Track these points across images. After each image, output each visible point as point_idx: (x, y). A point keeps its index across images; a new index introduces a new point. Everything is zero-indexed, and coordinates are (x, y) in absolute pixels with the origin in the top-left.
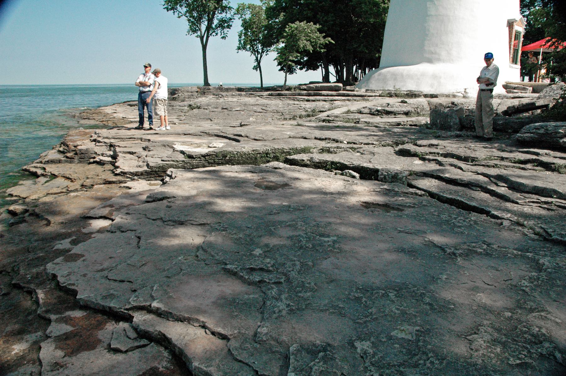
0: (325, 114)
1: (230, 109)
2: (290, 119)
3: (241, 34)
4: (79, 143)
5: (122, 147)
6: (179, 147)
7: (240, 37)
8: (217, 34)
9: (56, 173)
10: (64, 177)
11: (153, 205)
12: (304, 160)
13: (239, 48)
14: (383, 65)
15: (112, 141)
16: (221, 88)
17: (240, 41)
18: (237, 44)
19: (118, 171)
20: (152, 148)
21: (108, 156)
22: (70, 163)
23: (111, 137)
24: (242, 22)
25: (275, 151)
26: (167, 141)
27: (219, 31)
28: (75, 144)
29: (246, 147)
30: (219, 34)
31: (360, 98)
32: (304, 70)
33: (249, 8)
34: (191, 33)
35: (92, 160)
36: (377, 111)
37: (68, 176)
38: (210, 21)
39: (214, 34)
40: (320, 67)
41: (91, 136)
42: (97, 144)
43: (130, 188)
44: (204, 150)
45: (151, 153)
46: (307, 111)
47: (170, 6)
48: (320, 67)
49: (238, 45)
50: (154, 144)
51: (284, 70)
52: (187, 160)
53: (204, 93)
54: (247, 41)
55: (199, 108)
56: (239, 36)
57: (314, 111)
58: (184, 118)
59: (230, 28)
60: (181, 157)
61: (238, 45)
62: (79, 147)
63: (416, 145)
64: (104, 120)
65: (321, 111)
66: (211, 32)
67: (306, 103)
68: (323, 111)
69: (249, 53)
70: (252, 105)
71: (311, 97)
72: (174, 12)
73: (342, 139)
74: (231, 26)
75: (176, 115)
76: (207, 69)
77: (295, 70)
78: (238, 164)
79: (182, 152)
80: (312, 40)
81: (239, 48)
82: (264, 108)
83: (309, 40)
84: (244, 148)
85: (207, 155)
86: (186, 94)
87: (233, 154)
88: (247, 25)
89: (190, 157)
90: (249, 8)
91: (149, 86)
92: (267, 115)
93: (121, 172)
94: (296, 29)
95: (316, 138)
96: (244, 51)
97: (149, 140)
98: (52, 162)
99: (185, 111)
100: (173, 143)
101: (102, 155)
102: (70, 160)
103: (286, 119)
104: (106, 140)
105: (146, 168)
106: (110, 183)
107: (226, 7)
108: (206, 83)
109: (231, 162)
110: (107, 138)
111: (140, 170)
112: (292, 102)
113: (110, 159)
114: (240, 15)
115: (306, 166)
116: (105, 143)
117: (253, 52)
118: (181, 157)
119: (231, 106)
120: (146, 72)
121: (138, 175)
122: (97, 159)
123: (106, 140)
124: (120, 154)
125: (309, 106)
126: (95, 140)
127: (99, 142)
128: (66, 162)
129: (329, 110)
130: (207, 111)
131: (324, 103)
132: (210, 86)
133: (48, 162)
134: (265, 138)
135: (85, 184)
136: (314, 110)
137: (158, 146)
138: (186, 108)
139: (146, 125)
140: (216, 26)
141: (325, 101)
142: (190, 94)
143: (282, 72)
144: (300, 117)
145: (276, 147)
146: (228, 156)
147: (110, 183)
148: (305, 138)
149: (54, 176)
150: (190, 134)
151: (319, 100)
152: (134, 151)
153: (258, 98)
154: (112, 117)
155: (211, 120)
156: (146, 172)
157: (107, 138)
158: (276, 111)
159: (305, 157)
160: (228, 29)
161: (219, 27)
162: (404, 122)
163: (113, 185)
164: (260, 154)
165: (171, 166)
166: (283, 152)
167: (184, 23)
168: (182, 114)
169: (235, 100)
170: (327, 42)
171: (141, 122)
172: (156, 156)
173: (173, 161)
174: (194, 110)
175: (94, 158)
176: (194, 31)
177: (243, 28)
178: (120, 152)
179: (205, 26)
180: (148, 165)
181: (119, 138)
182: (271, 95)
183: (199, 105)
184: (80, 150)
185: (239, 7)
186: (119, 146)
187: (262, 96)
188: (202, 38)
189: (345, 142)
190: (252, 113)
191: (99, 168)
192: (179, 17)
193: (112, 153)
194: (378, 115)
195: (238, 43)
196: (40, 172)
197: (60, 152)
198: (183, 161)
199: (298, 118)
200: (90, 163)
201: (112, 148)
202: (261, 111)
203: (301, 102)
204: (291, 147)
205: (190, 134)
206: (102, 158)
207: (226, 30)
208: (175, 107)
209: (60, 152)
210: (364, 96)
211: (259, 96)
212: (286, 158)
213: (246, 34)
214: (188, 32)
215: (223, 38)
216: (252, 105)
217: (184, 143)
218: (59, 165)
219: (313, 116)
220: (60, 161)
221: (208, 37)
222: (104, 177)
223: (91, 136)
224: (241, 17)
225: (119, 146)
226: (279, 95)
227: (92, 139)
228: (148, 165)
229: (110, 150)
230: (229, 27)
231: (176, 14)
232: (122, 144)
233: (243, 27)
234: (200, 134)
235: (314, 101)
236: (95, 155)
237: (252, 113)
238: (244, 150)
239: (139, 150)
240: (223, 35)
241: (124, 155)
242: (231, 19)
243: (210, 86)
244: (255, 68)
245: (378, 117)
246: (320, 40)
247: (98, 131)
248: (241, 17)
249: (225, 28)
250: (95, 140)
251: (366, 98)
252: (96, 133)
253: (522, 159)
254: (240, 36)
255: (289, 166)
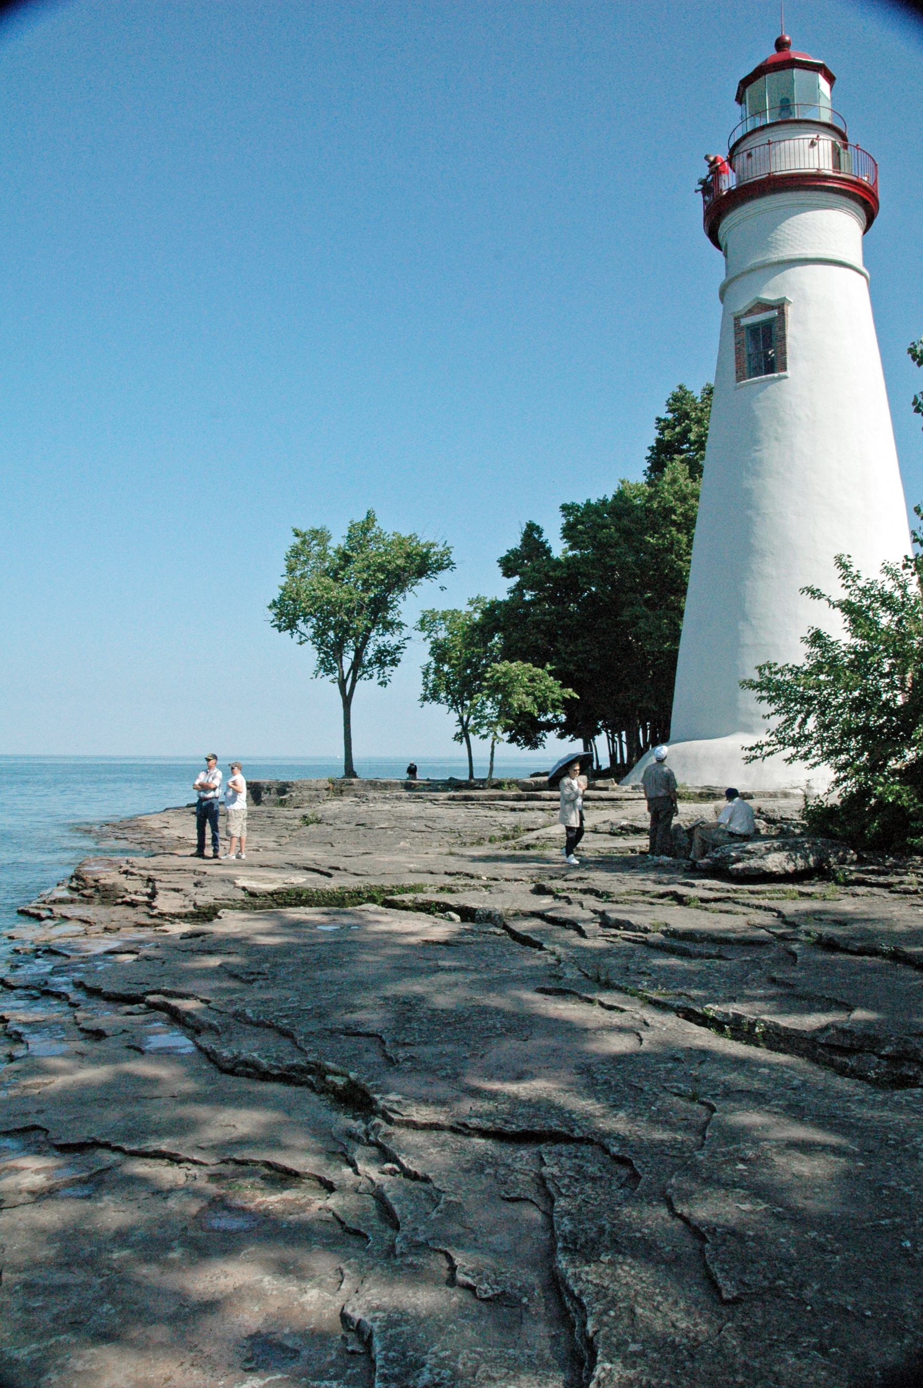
0: (534, 834)
1: (369, 826)
2: (472, 844)
3: (428, 671)
4: (101, 876)
5: (164, 880)
6: (241, 883)
7: (425, 677)
8: (371, 677)
9: (69, 915)
10: (80, 920)
11: (188, 941)
12: (404, 901)
13: (425, 698)
14: (675, 738)
15: (152, 873)
16: (373, 785)
17: (425, 684)
18: (421, 690)
19: (155, 912)
20: (206, 884)
21: (143, 895)
22: (88, 903)
23: (150, 867)
24: (431, 646)
25: (369, 888)
26: (228, 875)
27: (375, 671)
28: (96, 877)
29: (332, 884)
30: (376, 676)
31: (606, 803)
32: (569, 738)
33: (444, 618)
34: (322, 673)
35: (120, 900)
36: (622, 828)
37: (85, 918)
38: (359, 653)
39: (365, 676)
40: (604, 733)
41: (121, 867)
42: (130, 877)
43: (166, 931)
44: (271, 887)
45: (203, 890)
46: (504, 830)
47: (284, 622)
48: (604, 733)
49: (423, 692)
50: (210, 878)
51: (518, 741)
52: (248, 899)
53: (342, 791)
54: (439, 685)
55: (319, 822)
56: (424, 673)
57: (516, 829)
58: (288, 840)
59: (396, 665)
60: (241, 895)
61: (423, 692)
62: (102, 881)
63: (566, 880)
64: (143, 840)
65: (529, 830)
66: (359, 673)
67: (508, 814)
68: (533, 830)
69: (445, 708)
70: (411, 818)
71: (522, 803)
72: (292, 634)
73: (480, 873)
74: (399, 661)
75: (276, 835)
76: (350, 744)
77: (541, 740)
78: (318, 905)
79: (244, 889)
80: (538, 694)
81: (425, 698)
82: (430, 824)
83: (533, 694)
84: (329, 884)
85: (276, 893)
86: (306, 793)
87: (311, 892)
88: (440, 652)
89: (252, 894)
90: (444, 618)
91: (214, 789)
92: (432, 836)
93: (159, 913)
94: (505, 674)
95: (446, 873)
96: (434, 703)
97: (205, 873)
98: (61, 901)
99: (292, 828)
100: (236, 877)
101: (136, 893)
102: (88, 899)
103: (465, 844)
104: (143, 872)
105: (192, 909)
106: (143, 925)
107: (391, 624)
108: (350, 771)
109: (306, 903)
110: (144, 868)
111: (184, 910)
112: (482, 812)
113: (146, 899)
114: (427, 632)
115: (406, 908)
116: (141, 875)
117: (452, 706)
118: (241, 895)
119: (374, 821)
120: (210, 767)
121: (181, 918)
122: (128, 899)
123: (143, 872)
124: (161, 892)
125: (509, 819)
126: (126, 872)
127: (132, 874)
128: (81, 902)
129: (544, 827)
130: (329, 829)
131: (540, 813)
132: (355, 777)
133: (54, 902)
134: (371, 872)
135: (109, 926)
136: (516, 827)
137: (216, 881)
138: (297, 822)
139: (209, 852)
140: (369, 660)
141: (542, 810)
142: (314, 793)
143: (514, 744)
144: (490, 841)
145: (373, 884)
146: (305, 895)
147: (143, 925)
148: (432, 873)
149: (66, 918)
150: (268, 866)
151: (533, 809)
152: (180, 887)
153: (428, 804)
154: (159, 835)
155: (332, 846)
156: (192, 913)
157: (144, 868)
158: (448, 830)
159: (407, 898)
160: (393, 668)
161: (376, 662)
162: (640, 846)
163: (146, 929)
164: (348, 892)
165: (226, 907)
166: (382, 891)
167: (310, 655)
168: (286, 833)
169: (387, 807)
170: (567, 696)
171: (201, 846)
172: (209, 894)
173: (229, 900)
174: (311, 826)
175: (124, 897)
176: (330, 670)
177: (432, 659)
178: (161, 888)
179: (350, 661)
180: (195, 905)
181: (162, 870)
182: (453, 799)
183: (320, 816)
184: (104, 885)
185: (425, 617)
186: (160, 881)
187: (437, 800)
188: (342, 683)
189: (484, 878)
190: (405, 833)
191: (129, 911)
192: (301, 643)
193: (149, 890)
194: (621, 834)
195: (423, 687)
196: (44, 913)
197: (71, 888)
198: (243, 900)
199: (486, 843)
200: (117, 904)
201: (151, 884)
202: (424, 829)
203: (501, 813)
204: (394, 884)
205: (268, 866)
206: (134, 897)
207: (387, 669)
208: (276, 820)
209: (71, 888)
210: (617, 800)
211: (431, 801)
212: (385, 900)
213: (437, 671)
214: (316, 673)
215: (381, 684)
216: (411, 818)
217: (251, 878)
218: (71, 906)
219: (513, 838)
220: (72, 901)
221: (354, 681)
222: (134, 919)
223: (121, 867)
224: (429, 637)
225: (160, 881)
226: (467, 798)
227: (122, 870)
228: (195, 905)
229: (147, 886)
230: (394, 662)
231: (296, 636)
232: (165, 877)
233: (433, 655)
234: (285, 866)
235: (523, 810)
236: (124, 893)
237: (405, 833)
238: (328, 887)
239: (189, 887)
240: (381, 679)
241: (166, 893)
242: (398, 648)
243: (355, 777)
244: (458, 737)
245: (621, 839)
246: (553, 692)
247: (132, 859)
248: (429, 637)
249: (386, 665)
250: (126, 872)
251: (619, 803)
252: (128, 862)
253: (661, 891)
254: (426, 674)
255: (384, 909)
